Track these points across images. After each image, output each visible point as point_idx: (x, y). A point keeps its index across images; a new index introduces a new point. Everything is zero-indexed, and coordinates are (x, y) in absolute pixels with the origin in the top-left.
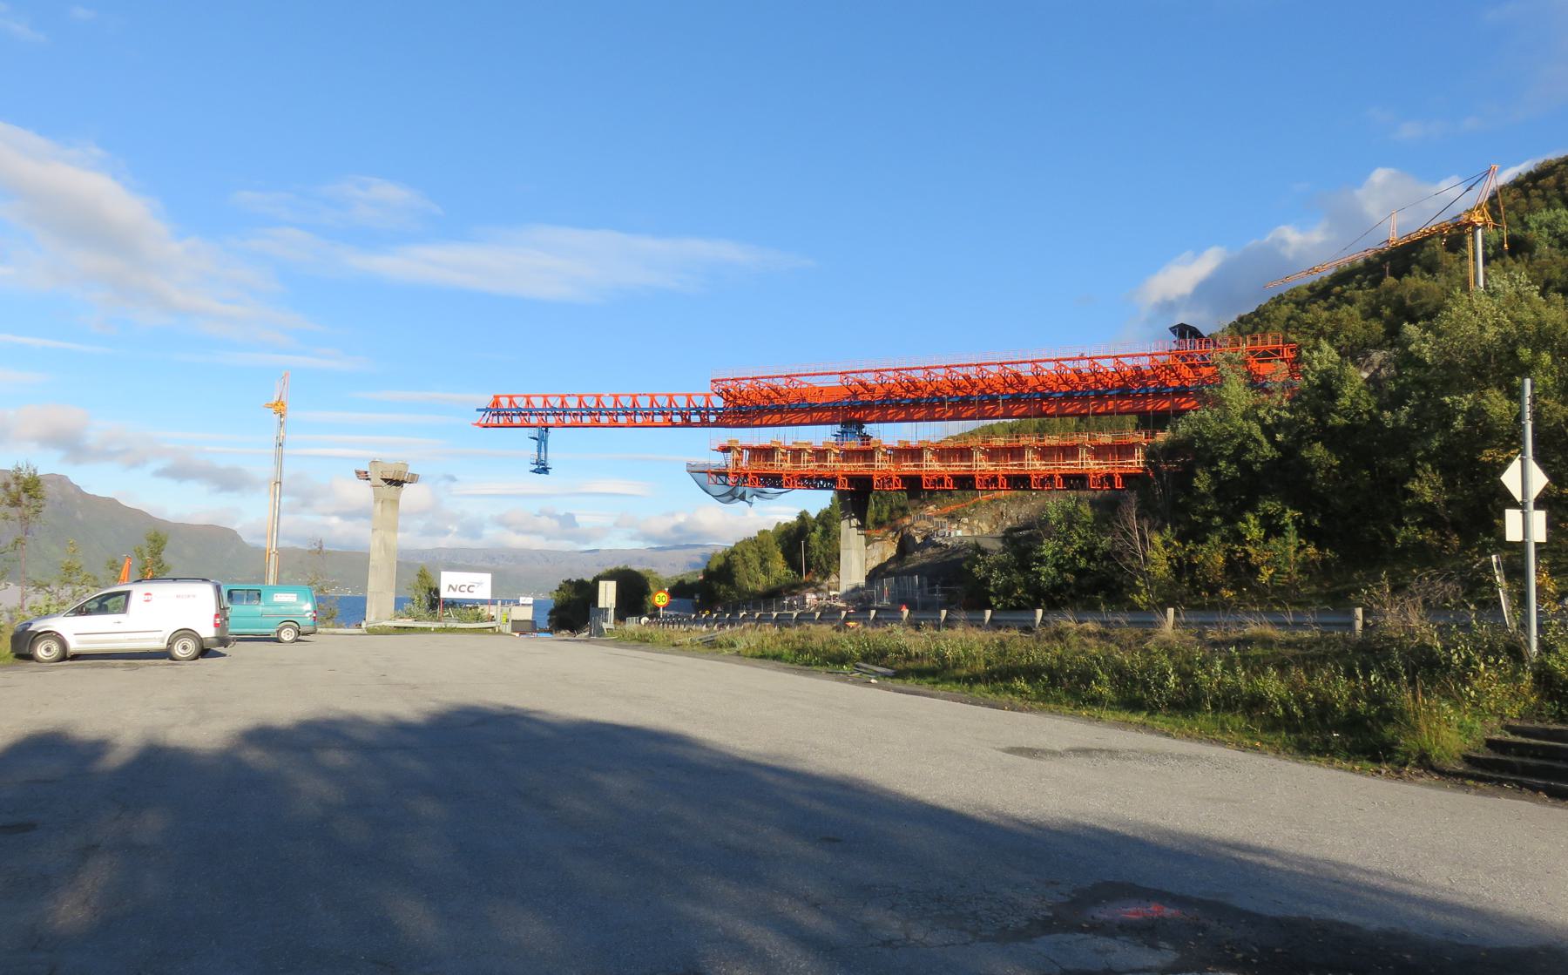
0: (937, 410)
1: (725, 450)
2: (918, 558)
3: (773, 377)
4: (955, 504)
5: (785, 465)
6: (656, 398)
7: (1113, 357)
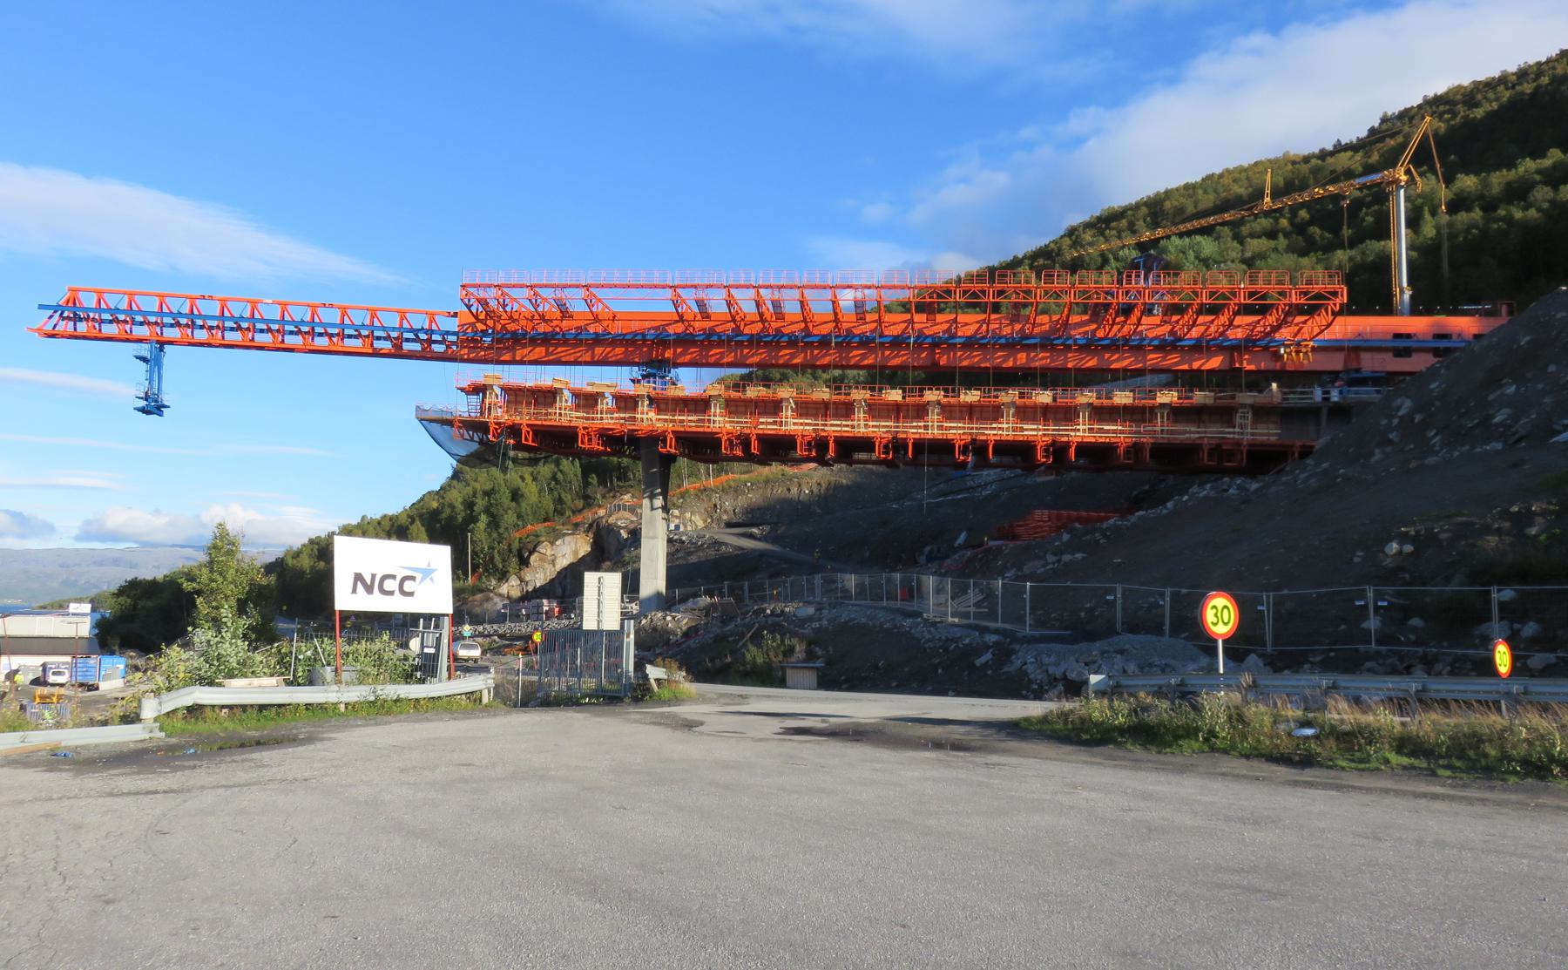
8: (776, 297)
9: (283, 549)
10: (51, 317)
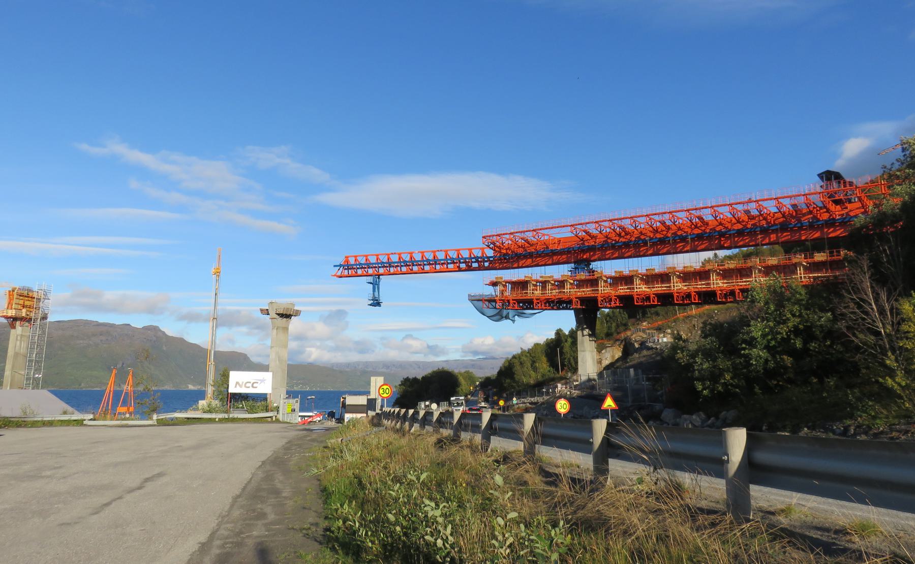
0: (641, 249)
1: (494, 284)
2: (636, 358)
3: (524, 232)
4: (661, 320)
5: (536, 292)
6: (448, 252)
7: (775, 199)
8: (793, 203)
9: (503, 361)
10: (339, 269)
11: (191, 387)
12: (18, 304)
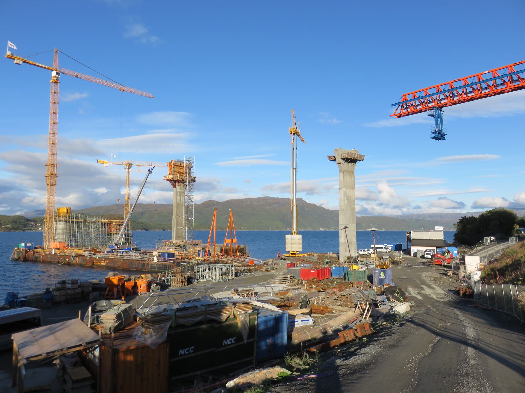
11: (321, 229)
12: (175, 171)
